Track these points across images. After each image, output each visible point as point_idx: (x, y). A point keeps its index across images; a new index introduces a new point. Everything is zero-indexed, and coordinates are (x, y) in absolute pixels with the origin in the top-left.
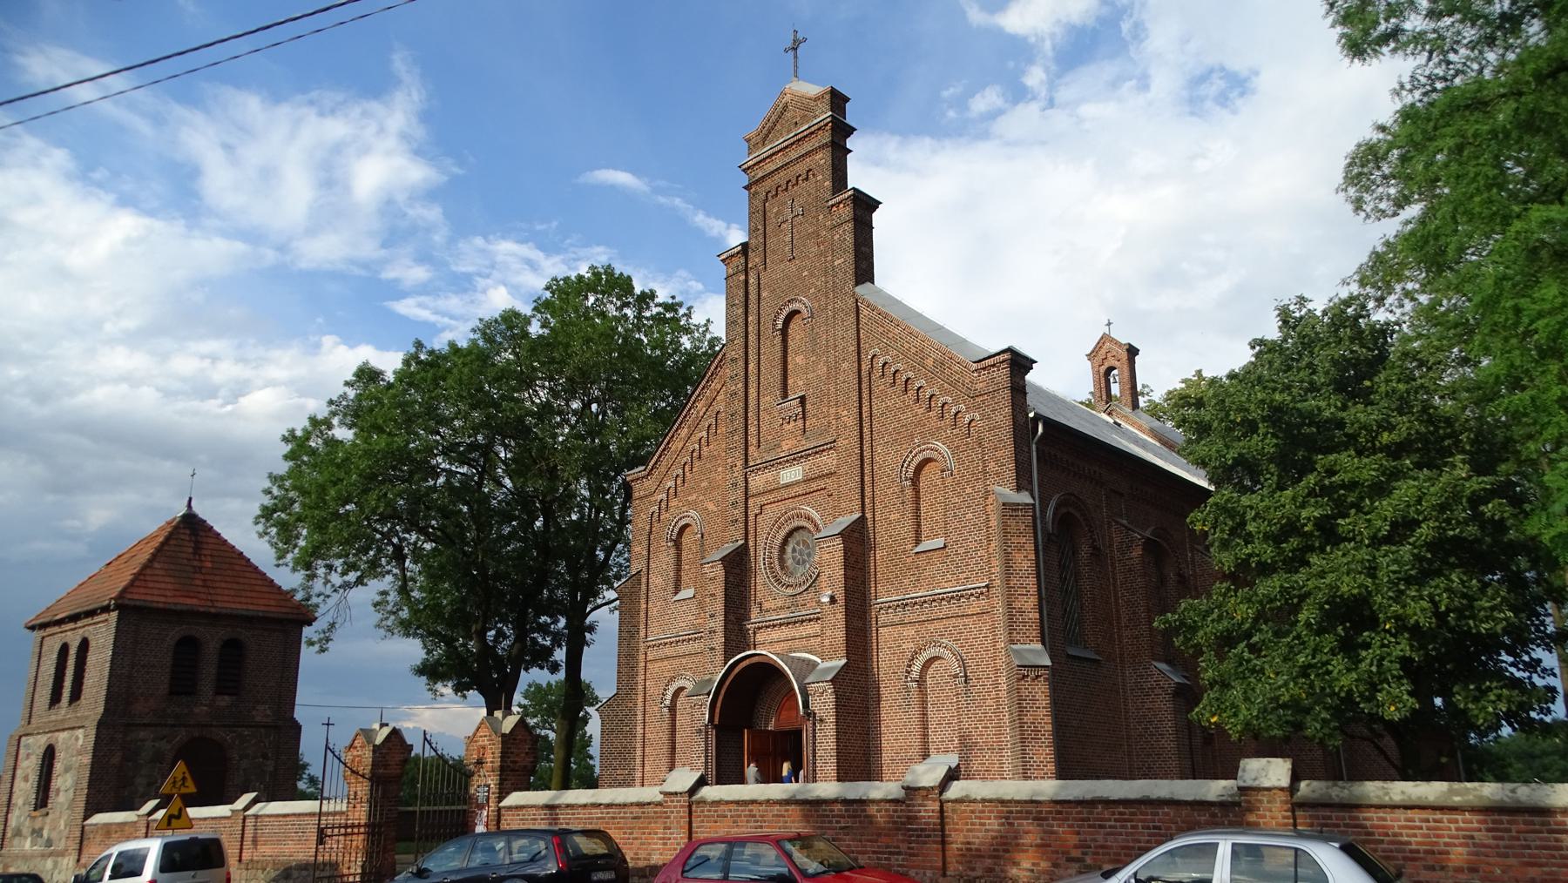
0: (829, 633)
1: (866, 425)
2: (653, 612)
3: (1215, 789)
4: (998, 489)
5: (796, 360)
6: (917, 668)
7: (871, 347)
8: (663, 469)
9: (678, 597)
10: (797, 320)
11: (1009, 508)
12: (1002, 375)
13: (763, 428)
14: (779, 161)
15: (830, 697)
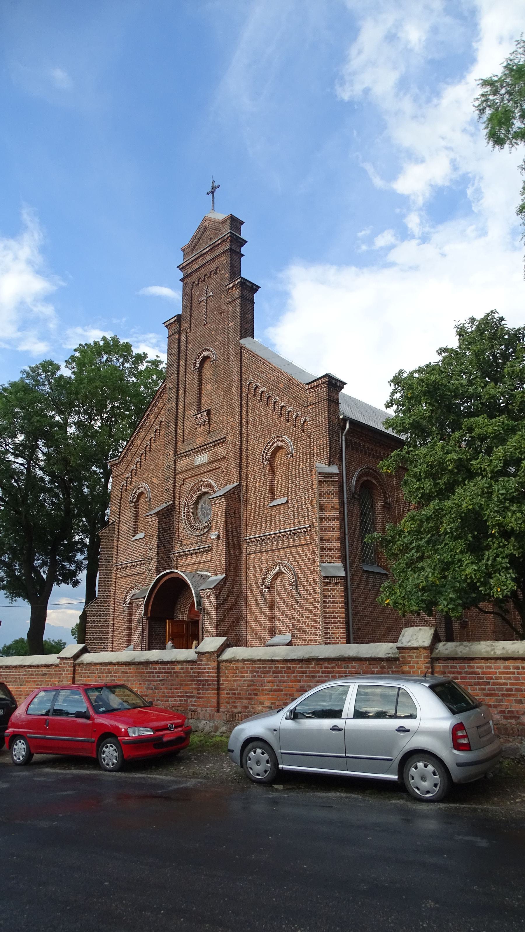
0: (215, 558)
1: (244, 427)
2: (121, 547)
3: (383, 649)
4: (318, 464)
5: (207, 387)
6: (268, 580)
8: (129, 458)
11: (324, 476)
12: (323, 392)
13: (186, 431)
14: (200, 262)
15: (213, 599)
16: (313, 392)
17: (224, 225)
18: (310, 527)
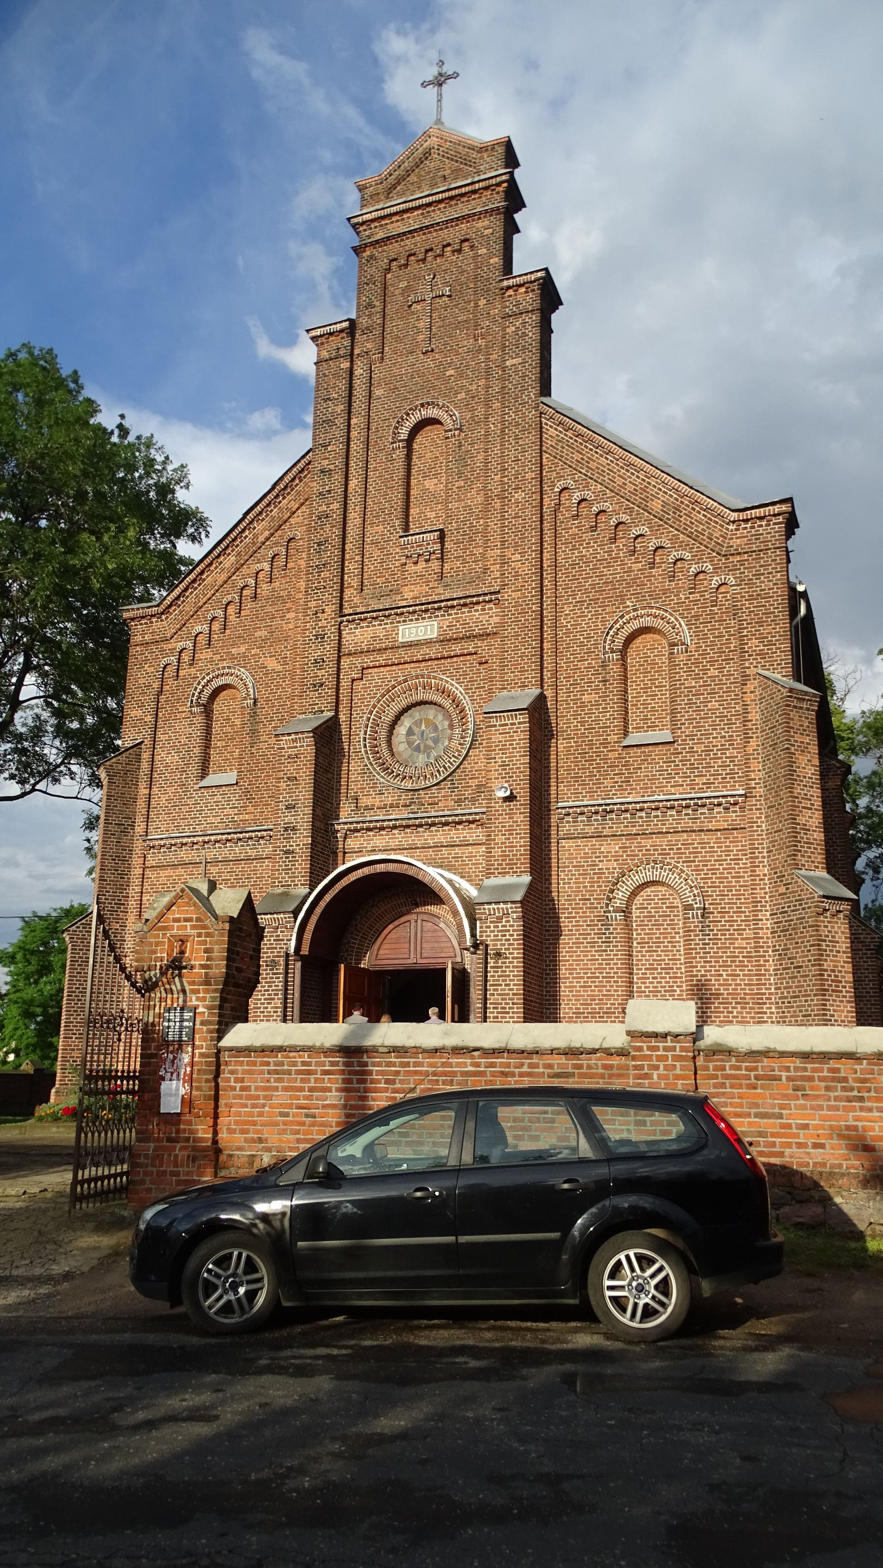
0: (500, 839)
2: (161, 799)
6: (621, 895)
7: (560, 477)
9: (205, 782)
10: (429, 432)
13: (370, 567)
14: (414, 221)
16: (746, 528)
17: (485, 155)
18: (745, 796)
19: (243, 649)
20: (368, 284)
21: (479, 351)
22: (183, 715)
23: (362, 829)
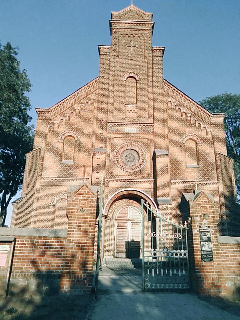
14: (127, 26)
19: (76, 126)
20: (114, 38)
21: (146, 63)
22: (55, 142)
23: (115, 181)
